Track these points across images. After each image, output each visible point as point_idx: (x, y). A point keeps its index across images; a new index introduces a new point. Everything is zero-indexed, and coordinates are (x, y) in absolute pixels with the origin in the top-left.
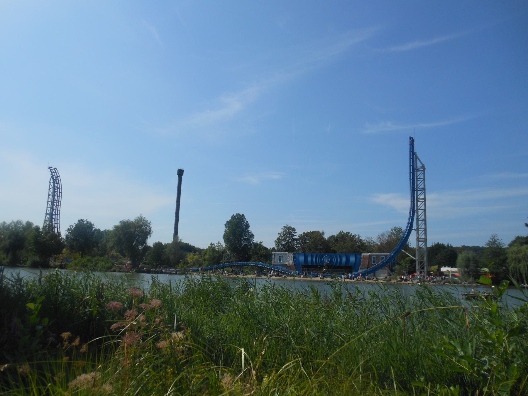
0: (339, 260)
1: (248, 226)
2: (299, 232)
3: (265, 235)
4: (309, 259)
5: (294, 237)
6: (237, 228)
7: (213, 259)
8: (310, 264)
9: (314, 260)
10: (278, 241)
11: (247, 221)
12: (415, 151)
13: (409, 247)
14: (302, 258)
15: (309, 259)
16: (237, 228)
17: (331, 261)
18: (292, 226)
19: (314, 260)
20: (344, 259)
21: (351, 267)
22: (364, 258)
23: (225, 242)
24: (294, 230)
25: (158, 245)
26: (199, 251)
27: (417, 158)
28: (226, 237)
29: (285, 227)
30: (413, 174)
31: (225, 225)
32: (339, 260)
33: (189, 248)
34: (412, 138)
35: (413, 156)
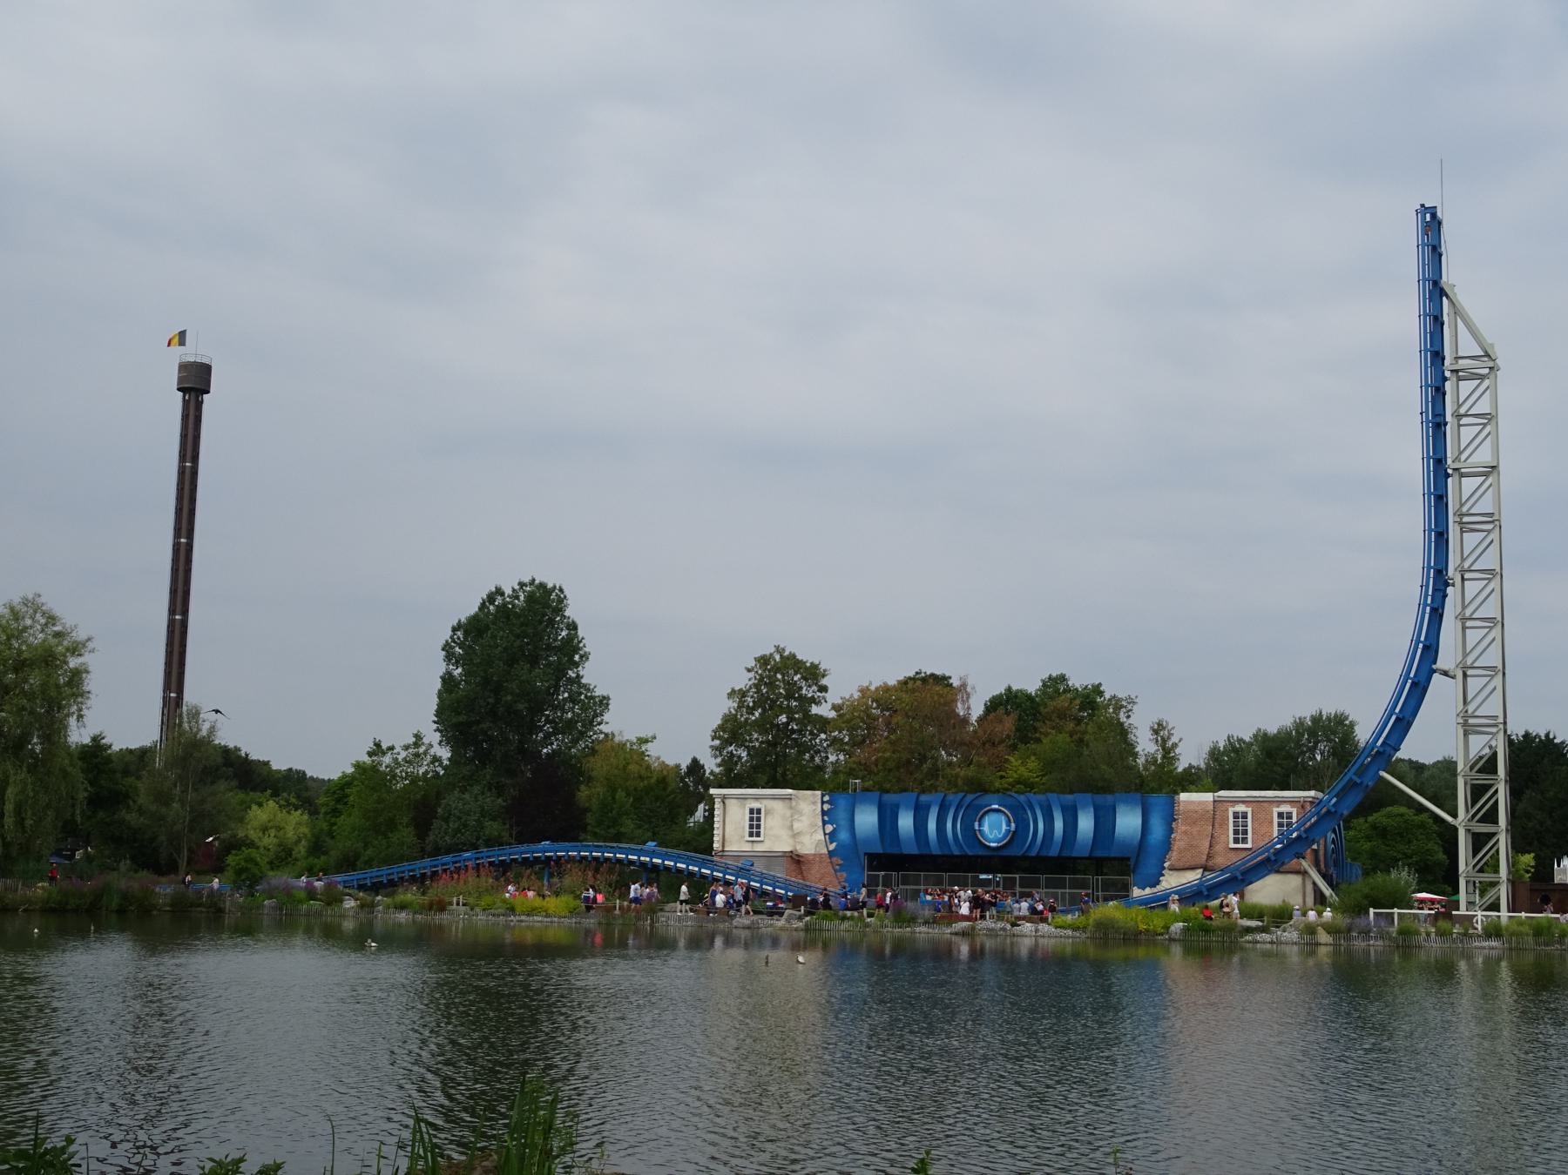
0: (1059, 825)
1: (571, 650)
2: (844, 684)
3: (657, 697)
4: (906, 822)
5: (815, 710)
6: (515, 659)
7: (374, 834)
8: (911, 849)
9: (932, 826)
10: (730, 731)
11: (573, 627)
12: (1447, 279)
13: (109, 759)
14: (867, 819)
15: (906, 822)
16: (515, 659)
17: (1015, 837)
18: (806, 655)
19: (932, 826)
20: (1086, 823)
21: (1124, 860)
22: (1195, 817)
23: (66, 727)
24: (813, 674)
25: (95, 752)
26: (292, 787)
27: (1457, 311)
28: (456, 711)
29: (763, 661)
30: (1440, 392)
31: (447, 648)
32: (1059, 825)
33: (247, 775)
34: (1433, 212)
35: (1435, 291)
